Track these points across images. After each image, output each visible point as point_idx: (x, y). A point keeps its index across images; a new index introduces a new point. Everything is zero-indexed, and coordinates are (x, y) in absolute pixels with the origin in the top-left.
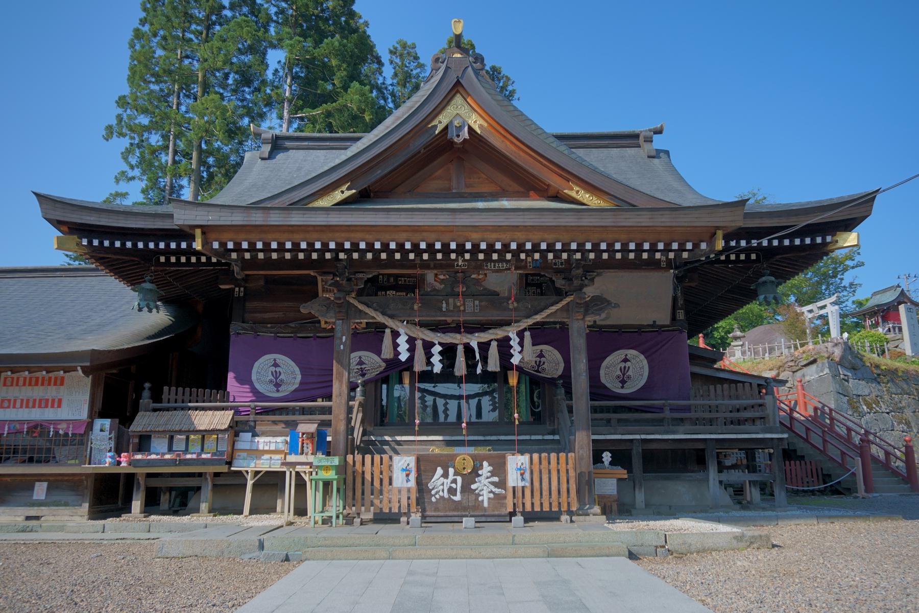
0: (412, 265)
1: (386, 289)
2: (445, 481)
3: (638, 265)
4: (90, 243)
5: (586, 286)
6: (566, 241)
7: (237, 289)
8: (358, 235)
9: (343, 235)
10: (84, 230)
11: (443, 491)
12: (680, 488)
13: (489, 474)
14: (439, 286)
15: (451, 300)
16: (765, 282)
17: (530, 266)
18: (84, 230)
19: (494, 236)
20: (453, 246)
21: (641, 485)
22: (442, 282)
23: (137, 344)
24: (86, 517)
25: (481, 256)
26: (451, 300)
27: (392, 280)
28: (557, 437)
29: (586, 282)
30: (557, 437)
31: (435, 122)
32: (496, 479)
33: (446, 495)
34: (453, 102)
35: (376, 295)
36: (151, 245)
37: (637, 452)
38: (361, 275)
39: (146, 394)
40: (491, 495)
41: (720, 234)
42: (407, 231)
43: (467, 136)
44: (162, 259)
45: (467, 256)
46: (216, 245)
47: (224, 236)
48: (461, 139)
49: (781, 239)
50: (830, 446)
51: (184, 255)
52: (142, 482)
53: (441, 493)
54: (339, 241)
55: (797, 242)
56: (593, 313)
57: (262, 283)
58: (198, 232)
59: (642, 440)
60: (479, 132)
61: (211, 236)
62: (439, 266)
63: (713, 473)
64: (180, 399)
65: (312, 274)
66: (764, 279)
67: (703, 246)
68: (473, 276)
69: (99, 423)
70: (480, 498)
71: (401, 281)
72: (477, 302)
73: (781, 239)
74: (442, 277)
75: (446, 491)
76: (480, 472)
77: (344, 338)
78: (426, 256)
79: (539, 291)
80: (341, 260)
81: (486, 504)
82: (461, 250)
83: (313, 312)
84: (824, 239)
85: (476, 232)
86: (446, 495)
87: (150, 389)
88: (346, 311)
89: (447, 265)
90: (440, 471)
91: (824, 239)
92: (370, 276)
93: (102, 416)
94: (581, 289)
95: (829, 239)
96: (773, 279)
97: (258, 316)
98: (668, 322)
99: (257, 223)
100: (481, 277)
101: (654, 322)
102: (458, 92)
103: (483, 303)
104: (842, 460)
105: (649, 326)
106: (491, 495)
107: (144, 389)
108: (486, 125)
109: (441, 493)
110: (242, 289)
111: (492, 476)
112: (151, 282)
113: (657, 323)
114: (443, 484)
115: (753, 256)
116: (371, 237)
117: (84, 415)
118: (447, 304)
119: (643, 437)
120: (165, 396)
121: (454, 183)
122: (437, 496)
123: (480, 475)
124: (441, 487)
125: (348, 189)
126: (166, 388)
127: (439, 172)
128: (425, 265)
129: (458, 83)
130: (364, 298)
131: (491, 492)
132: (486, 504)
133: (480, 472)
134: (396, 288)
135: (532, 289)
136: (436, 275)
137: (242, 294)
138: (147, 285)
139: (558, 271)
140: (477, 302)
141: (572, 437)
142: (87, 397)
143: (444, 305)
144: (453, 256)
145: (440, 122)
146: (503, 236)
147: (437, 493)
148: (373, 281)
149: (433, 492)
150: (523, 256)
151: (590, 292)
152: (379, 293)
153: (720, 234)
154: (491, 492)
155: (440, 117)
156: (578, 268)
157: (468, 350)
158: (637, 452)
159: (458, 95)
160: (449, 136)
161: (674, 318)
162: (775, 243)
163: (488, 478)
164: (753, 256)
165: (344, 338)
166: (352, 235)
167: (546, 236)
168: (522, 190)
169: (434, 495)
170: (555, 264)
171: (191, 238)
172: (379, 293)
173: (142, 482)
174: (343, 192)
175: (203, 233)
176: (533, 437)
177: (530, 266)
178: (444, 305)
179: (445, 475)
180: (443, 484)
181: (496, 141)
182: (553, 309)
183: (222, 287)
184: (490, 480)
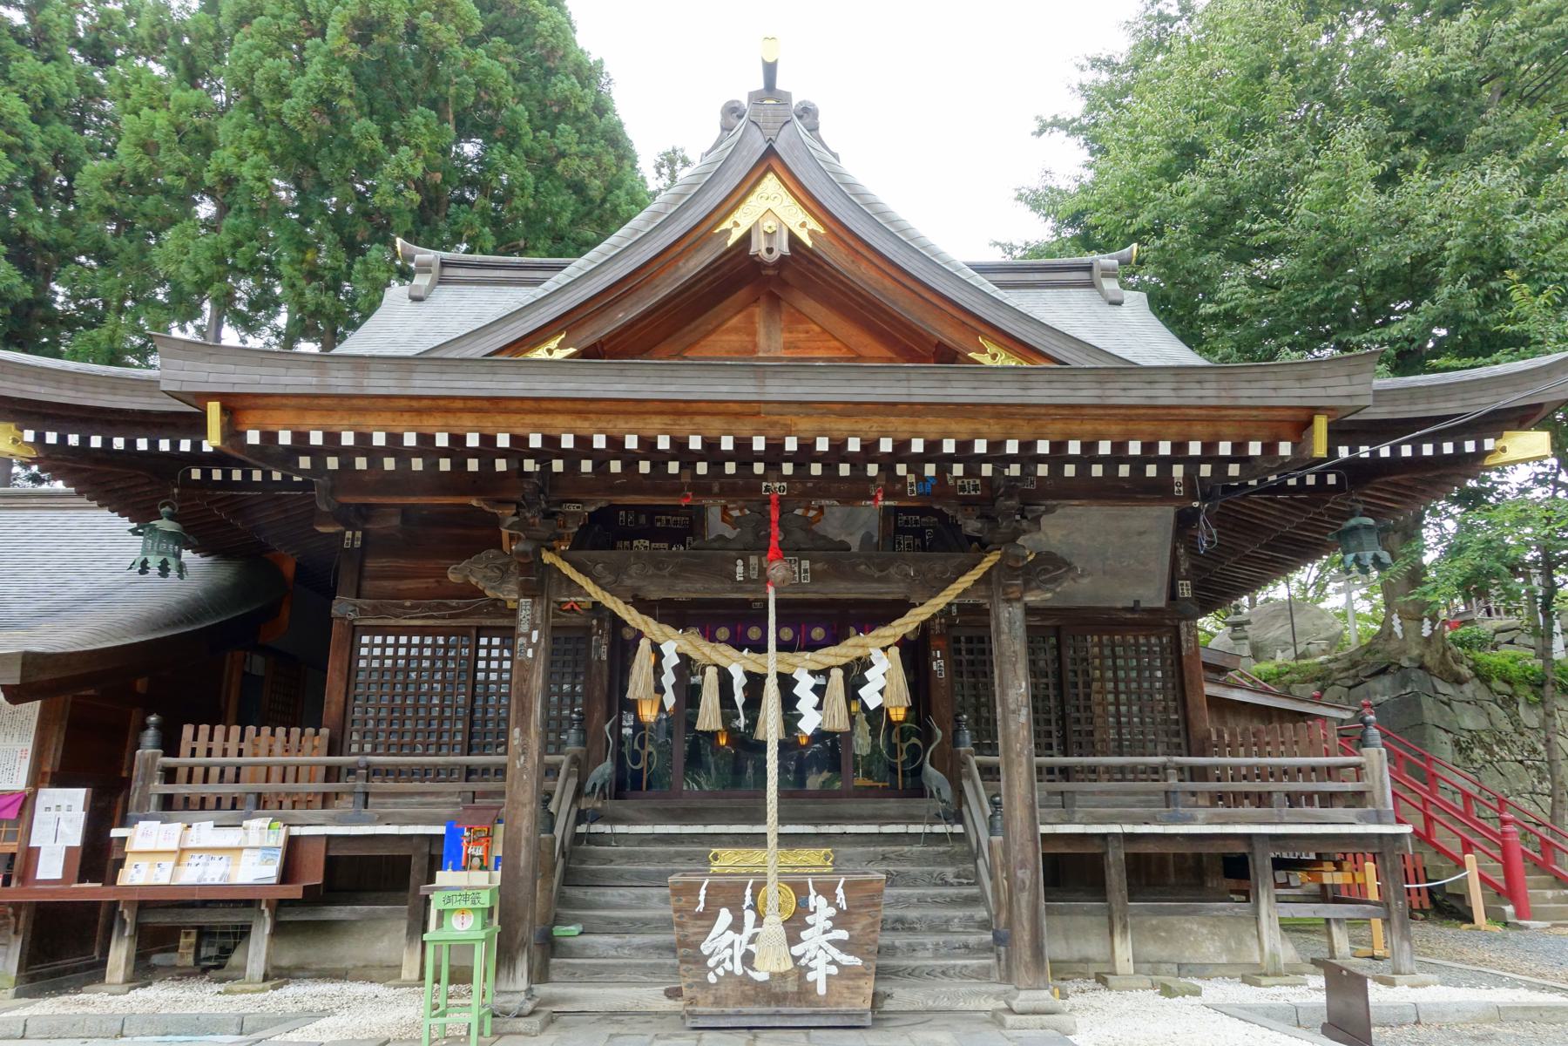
0: (673, 485)
1: (632, 534)
2: (737, 937)
3: (1110, 492)
4: (40, 438)
5: (1025, 532)
6: (997, 437)
7: (349, 534)
8: (560, 421)
9: (529, 419)
10: (22, 412)
11: (732, 959)
12: (1200, 932)
13: (829, 924)
14: (730, 533)
15: (753, 560)
16: (1355, 528)
17: (912, 491)
18: (30, 413)
19: (843, 425)
20: (759, 444)
21: (1125, 927)
22: (735, 523)
23: (136, 640)
24: (11, 991)
25: (816, 469)
26: (753, 560)
27: (643, 519)
28: (959, 829)
29: (1025, 523)
30: (959, 829)
31: (727, 225)
32: (843, 935)
33: (739, 970)
34: (759, 190)
35: (613, 547)
36: (142, 444)
37: (1116, 858)
38: (573, 508)
39: (150, 736)
40: (834, 970)
41: (1321, 424)
42: (662, 413)
43: (786, 250)
44: (196, 474)
45: (788, 468)
46: (253, 437)
47: (271, 420)
48: (776, 255)
49: (1416, 444)
50: (1438, 827)
51: (237, 467)
52: (128, 916)
53: (728, 965)
54: (519, 431)
55: (1448, 448)
56: (1039, 588)
57: (396, 521)
58: (214, 409)
59: (1125, 835)
60: (809, 243)
61: (250, 417)
62: (730, 489)
63: (1269, 911)
64: (201, 750)
65: (474, 503)
66: (1352, 522)
67: (1285, 449)
68: (799, 512)
69: (49, 796)
70: (810, 977)
71: (661, 522)
72: (806, 564)
73: (1416, 444)
74: (736, 513)
75: (738, 960)
76: (809, 919)
77: (535, 634)
78: (702, 468)
79: (918, 541)
80: (529, 474)
81: (821, 989)
82: (775, 453)
83: (473, 580)
84: (1479, 445)
85: (808, 415)
86: (739, 970)
87: (158, 727)
88: (538, 581)
89: (745, 487)
90: (725, 917)
91: (1479, 445)
92: (592, 509)
93: (63, 778)
94: (1014, 540)
95: (1489, 444)
96: (1371, 521)
97: (388, 585)
98: (1161, 603)
99: (340, 391)
100: (812, 513)
101: (1137, 602)
102: (770, 169)
103: (819, 566)
104: (1427, 828)
105: (1126, 609)
106: (834, 970)
107: (145, 727)
108: (821, 230)
109: (728, 965)
110: (359, 534)
111: (835, 927)
112: (171, 517)
113: (1143, 605)
114: (731, 946)
115: (1331, 479)
116: (586, 424)
117: (18, 781)
118: (746, 566)
119: (1128, 829)
120: (185, 747)
121: (762, 340)
122: (720, 971)
123: (808, 926)
124: (729, 951)
125: (561, 346)
126: (188, 730)
127: (734, 321)
128: (701, 486)
129: (770, 152)
130: (580, 555)
131: (833, 962)
132: (821, 989)
133: (809, 919)
134: (654, 535)
135: (907, 539)
136: (725, 509)
137: (358, 544)
138: (164, 525)
139: (967, 502)
140: (806, 564)
141: (853, 630)
142: (28, 745)
143: (740, 569)
144: (759, 468)
145: (736, 224)
146: (863, 426)
147: (719, 963)
148: (604, 517)
149: (711, 963)
150: (901, 469)
151: (1029, 545)
152: (619, 544)
153: (1321, 424)
154: (833, 962)
155: (738, 216)
156: (1010, 496)
157: (725, 679)
158: (1116, 858)
159: (771, 176)
160: (752, 251)
161: (1173, 595)
162: (1406, 451)
163: (825, 932)
164: (1331, 479)
165: (535, 634)
166: (546, 420)
167: (954, 426)
168: (890, 354)
169: (713, 969)
170: (963, 488)
171: (197, 425)
172: (619, 544)
173: (128, 916)
174: (550, 352)
175: (225, 410)
176: (913, 829)
177: (912, 491)
178: (740, 569)
179: (737, 926)
180: (731, 946)
181: (837, 257)
182: (966, 581)
183: (321, 529)
184: (830, 936)
